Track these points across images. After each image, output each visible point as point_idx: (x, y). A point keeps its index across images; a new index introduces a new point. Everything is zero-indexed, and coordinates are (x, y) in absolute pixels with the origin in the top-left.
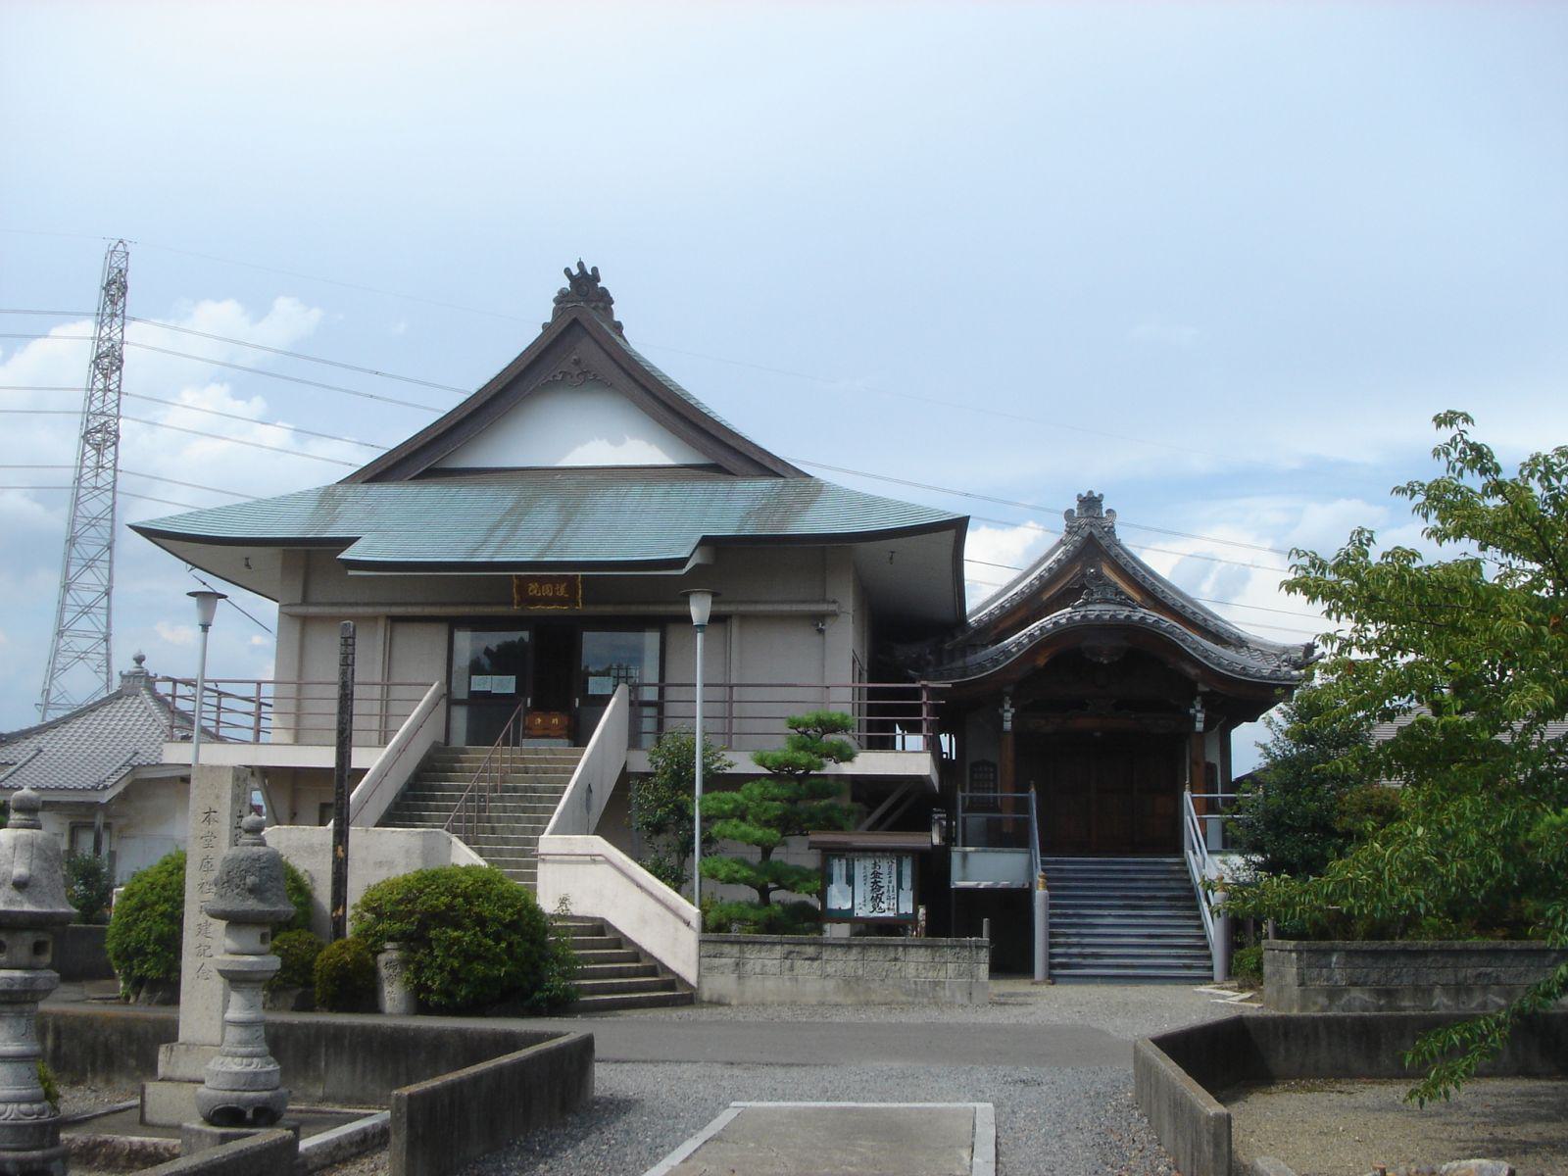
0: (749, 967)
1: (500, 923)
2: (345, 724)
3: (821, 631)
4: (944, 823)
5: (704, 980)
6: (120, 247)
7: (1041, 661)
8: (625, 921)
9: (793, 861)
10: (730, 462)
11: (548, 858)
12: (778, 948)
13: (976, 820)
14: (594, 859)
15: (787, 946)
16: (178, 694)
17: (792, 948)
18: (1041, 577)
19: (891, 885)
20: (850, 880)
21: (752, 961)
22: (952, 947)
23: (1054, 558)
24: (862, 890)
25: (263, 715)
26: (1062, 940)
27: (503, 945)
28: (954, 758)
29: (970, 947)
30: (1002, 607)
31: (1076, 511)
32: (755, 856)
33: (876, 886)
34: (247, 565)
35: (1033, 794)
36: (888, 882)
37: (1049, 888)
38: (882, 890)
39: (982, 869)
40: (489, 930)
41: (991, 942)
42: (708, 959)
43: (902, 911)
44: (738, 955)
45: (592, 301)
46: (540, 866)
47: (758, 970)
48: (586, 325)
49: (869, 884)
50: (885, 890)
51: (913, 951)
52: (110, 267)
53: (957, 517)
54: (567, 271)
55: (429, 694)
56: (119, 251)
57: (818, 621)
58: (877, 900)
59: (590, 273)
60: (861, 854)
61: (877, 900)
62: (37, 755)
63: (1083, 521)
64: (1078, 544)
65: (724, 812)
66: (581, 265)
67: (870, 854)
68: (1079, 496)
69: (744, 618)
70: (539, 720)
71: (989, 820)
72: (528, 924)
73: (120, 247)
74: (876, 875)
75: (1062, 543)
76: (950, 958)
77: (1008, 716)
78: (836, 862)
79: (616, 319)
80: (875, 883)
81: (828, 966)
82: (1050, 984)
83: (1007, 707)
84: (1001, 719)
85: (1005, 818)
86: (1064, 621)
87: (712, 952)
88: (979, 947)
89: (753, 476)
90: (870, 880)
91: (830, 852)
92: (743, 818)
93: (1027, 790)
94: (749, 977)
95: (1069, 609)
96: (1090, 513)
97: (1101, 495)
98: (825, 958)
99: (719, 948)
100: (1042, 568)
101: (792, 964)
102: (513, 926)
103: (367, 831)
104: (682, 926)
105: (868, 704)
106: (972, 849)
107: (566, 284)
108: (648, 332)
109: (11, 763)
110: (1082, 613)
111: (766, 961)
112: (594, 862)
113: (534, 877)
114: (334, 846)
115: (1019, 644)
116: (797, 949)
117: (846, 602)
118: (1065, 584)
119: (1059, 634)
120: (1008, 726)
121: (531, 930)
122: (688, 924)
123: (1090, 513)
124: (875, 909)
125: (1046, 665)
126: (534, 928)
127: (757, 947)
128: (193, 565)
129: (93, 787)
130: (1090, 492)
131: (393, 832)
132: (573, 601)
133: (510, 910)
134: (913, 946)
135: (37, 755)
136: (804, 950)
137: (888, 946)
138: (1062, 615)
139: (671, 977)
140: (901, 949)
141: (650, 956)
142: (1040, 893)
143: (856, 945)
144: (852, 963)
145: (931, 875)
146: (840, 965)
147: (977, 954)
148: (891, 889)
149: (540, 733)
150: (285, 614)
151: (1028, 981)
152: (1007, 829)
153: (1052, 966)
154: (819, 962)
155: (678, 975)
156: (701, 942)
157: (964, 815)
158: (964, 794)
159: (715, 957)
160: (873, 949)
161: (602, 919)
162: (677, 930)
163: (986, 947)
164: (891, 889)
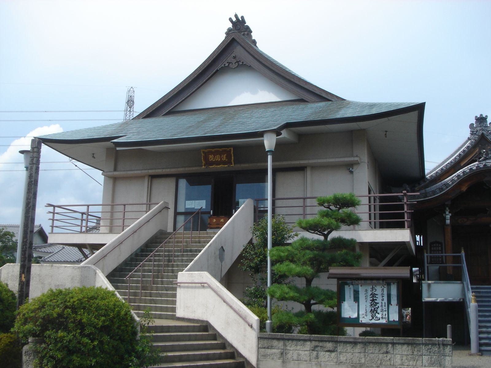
0: (289, 356)
1: (95, 327)
2: (30, 199)
3: (351, 172)
4: (418, 276)
5: (261, 363)
6: (132, 89)
7: (464, 189)
8: (218, 324)
9: (324, 287)
10: (306, 96)
11: (182, 285)
12: (308, 343)
13: (434, 268)
14: (203, 285)
15: (313, 342)
16: (56, 212)
17: (317, 343)
18: (464, 151)
19: (383, 302)
20: (356, 299)
21: (291, 352)
22: (426, 344)
23: (466, 146)
24: (365, 305)
25: (89, 220)
26: (484, 330)
27: (96, 343)
28: (422, 245)
29: (439, 345)
30: (442, 169)
31: (475, 124)
32: (301, 283)
33: (373, 302)
34: (93, 157)
35: (463, 254)
36: (381, 300)
37: (477, 301)
38: (378, 305)
39: (438, 292)
40: (87, 332)
41: (453, 342)
42: (263, 350)
43: (391, 319)
44: (282, 348)
45: (242, 32)
46: (178, 289)
47: (295, 358)
48: (254, 67)
49: (369, 302)
50: (379, 305)
51: (398, 347)
52: (129, 96)
53: (418, 103)
54: (230, 19)
55: (156, 206)
56: (131, 90)
57: (349, 167)
58: (374, 311)
59: (241, 19)
60: (363, 282)
61: (374, 311)
62: (62, 249)
63: (478, 129)
64: (477, 139)
65: (281, 257)
66: (236, 16)
67: (369, 282)
68: (476, 117)
69: (314, 167)
70: (215, 220)
71: (440, 266)
72: (119, 328)
73: (132, 89)
74: (373, 295)
75: (469, 139)
76: (425, 352)
77: (448, 217)
78: (346, 287)
79: (253, 39)
80: (373, 300)
81: (341, 356)
82: (480, 355)
83: (447, 213)
84: (445, 219)
85: (448, 266)
86: (475, 168)
87: (266, 345)
88: (445, 345)
89: (317, 102)
90: (369, 299)
91: (343, 281)
92: (292, 261)
93: (460, 252)
94: (290, 362)
95: (477, 163)
96: (481, 125)
97: (487, 116)
98: (339, 351)
99: (270, 343)
100: (460, 151)
101: (317, 354)
102: (105, 329)
103: (52, 266)
104: (248, 328)
105: (380, 213)
106: (433, 282)
107: (230, 25)
108: (266, 43)
109: (52, 252)
110: (484, 164)
111: (301, 352)
112: (203, 287)
113: (175, 296)
114: (20, 274)
115: (452, 180)
116: (321, 344)
117: (363, 157)
118: (471, 158)
119: (473, 175)
120: (448, 222)
121: (120, 332)
122: (251, 326)
123: (481, 125)
124: (373, 318)
125: (466, 190)
126: (123, 331)
127: (295, 342)
128: (72, 158)
129: (77, 261)
130: (481, 115)
131: (65, 267)
132: (229, 163)
133: (103, 318)
134: (399, 344)
135: (62, 249)
136: (325, 345)
137: (381, 343)
138: (474, 165)
139: (241, 360)
140: (390, 346)
141: (232, 346)
142: (472, 306)
143: (360, 343)
144: (357, 355)
145: (409, 294)
146: (349, 356)
147: (444, 349)
148: (383, 304)
149: (216, 226)
150: (107, 177)
151: (467, 352)
152: (450, 272)
153: (480, 345)
154: (335, 353)
155: (246, 359)
156: (259, 338)
157: (428, 265)
158: (427, 255)
159: (268, 348)
160: (371, 345)
161: (207, 322)
162: (245, 330)
163: (449, 345)
164: (383, 304)
